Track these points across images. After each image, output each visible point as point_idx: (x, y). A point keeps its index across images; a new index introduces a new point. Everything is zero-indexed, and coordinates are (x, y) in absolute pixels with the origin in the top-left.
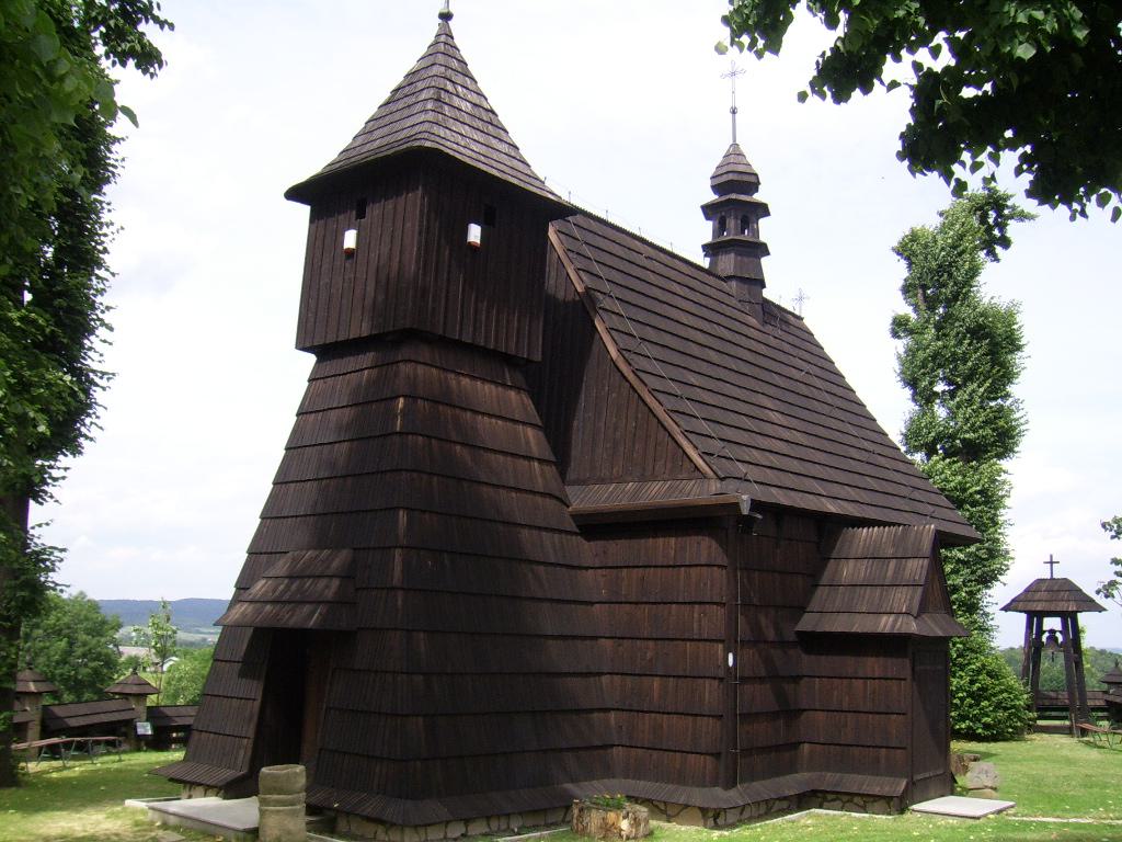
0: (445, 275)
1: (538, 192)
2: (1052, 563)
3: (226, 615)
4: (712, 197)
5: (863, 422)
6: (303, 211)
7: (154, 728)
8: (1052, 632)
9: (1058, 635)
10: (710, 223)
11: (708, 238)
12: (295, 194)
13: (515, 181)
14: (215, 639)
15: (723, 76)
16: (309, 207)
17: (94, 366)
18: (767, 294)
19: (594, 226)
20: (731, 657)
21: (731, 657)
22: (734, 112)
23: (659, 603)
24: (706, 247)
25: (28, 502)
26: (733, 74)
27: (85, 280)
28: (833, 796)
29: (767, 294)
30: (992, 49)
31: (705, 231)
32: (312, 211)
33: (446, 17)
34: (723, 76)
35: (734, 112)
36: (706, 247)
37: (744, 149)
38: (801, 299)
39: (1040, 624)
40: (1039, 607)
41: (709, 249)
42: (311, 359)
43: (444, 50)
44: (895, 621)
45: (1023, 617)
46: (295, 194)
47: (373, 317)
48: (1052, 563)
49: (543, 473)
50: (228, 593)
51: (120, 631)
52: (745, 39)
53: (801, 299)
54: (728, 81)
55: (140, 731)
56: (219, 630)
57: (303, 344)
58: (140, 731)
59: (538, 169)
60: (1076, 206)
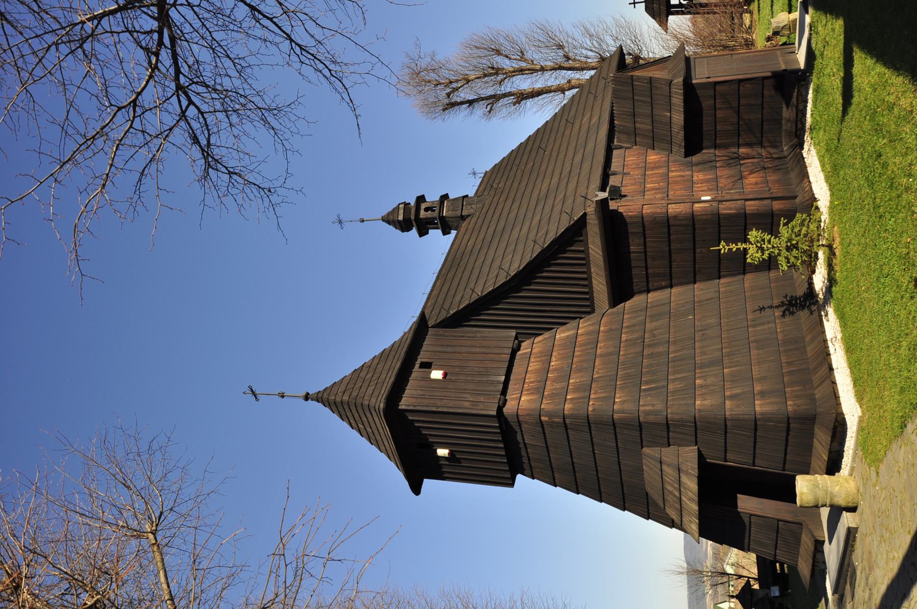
1: (411, 335)
2: (634, 3)
3: (693, 536)
4: (414, 232)
5: (549, 126)
6: (428, 484)
7: (774, 584)
10: (430, 231)
11: (439, 232)
12: (416, 489)
13: (393, 379)
14: (710, 542)
15: (342, 228)
18: (471, 194)
21: (703, 198)
24: (445, 233)
27: (798, 402)
28: (799, 123)
29: (471, 194)
30: (727, 209)
31: (435, 234)
33: (307, 397)
36: (445, 233)
37: (384, 213)
38: (474, 174)
39: (675, 6)
40: (664, 8)
41: (446, 232)
42: (519, 477)
43: (320, 398)
44: (687, 473)
45: (671, 18)
46: (416, 489)
47: (709, 422)
48: (634, 3)
50: (677, 535)
51: (820, 204)
54: (345, 225)
55: (777, 594)
56: (703, 540)
58: (777, 594)
59: (397, 337)
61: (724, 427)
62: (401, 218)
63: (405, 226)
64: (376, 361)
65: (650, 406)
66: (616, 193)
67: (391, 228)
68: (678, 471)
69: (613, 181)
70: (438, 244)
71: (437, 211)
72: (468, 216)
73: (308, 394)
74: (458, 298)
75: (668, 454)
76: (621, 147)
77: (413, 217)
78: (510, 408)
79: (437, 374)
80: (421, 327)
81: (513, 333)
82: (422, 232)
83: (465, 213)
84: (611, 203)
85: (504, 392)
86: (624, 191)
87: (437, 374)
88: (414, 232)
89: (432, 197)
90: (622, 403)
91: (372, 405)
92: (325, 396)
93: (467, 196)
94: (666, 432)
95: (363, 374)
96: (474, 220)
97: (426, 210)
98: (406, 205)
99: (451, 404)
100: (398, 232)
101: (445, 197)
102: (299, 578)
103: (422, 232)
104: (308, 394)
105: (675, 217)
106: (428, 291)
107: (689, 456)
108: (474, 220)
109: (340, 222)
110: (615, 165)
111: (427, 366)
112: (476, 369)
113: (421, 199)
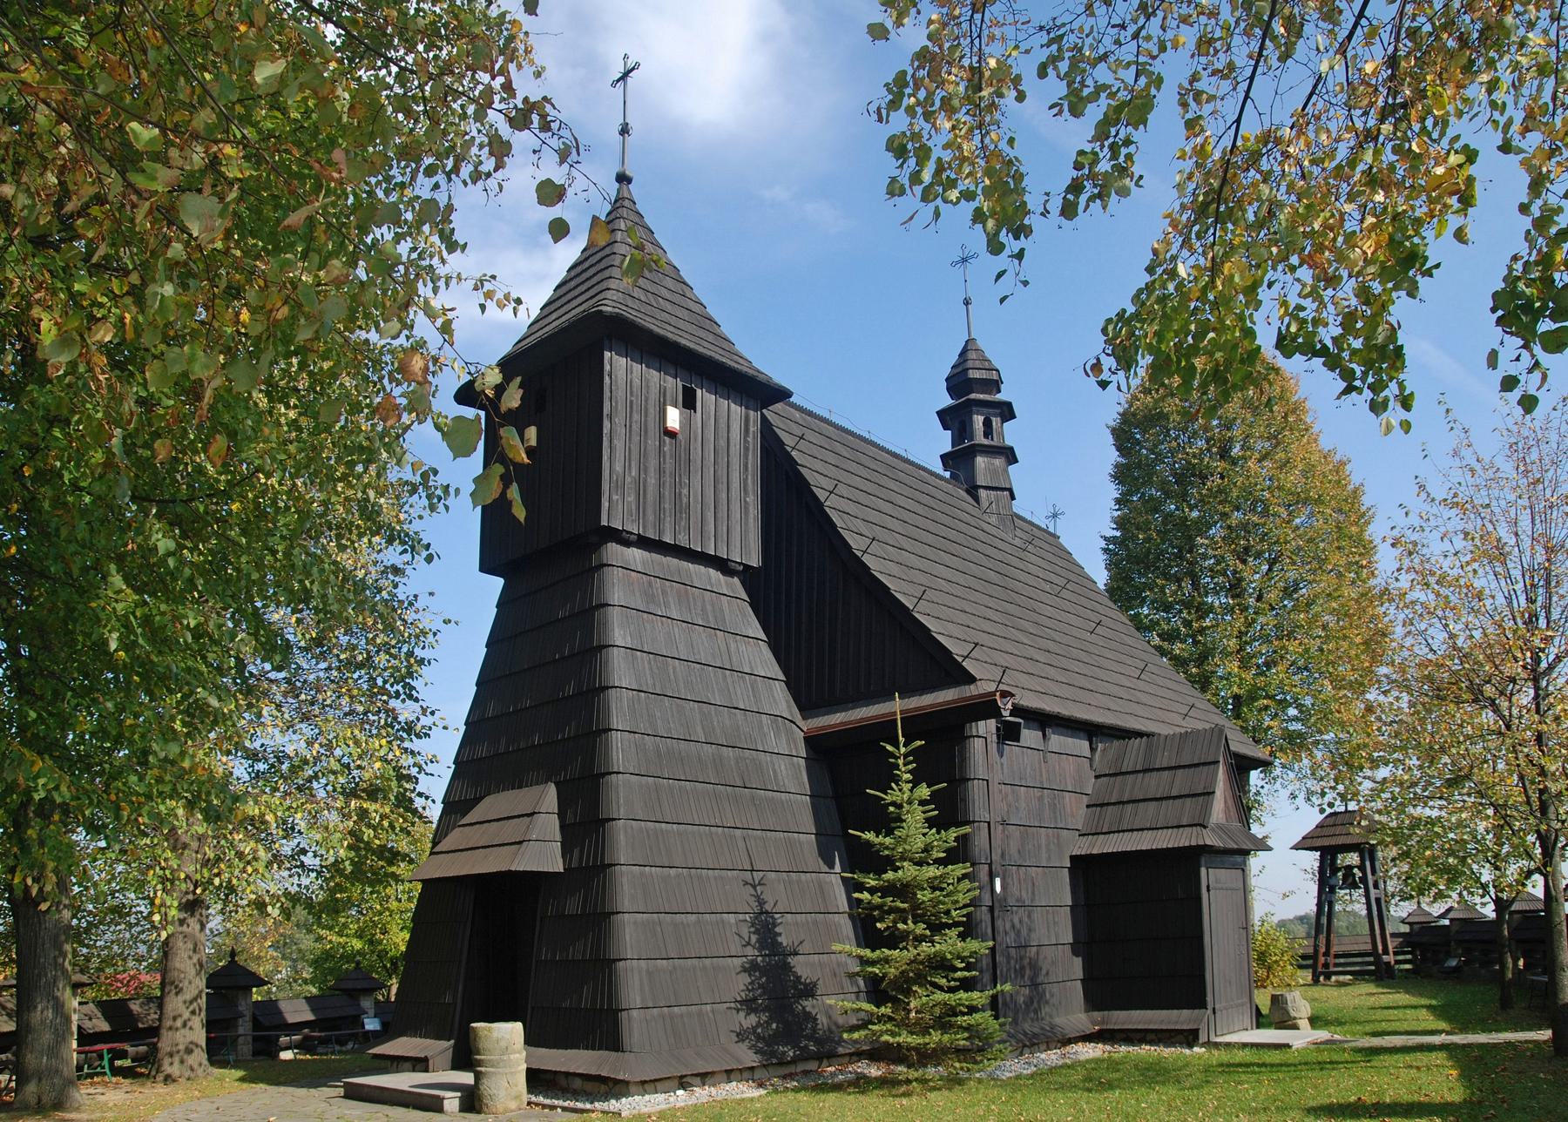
0: (455, 607)
4: (947, 401)
8: (1349, 868)
9: (1356, 870)
11: (948, 448)
12: (1270, 849)
15: (954, 264)
16: (519, 1026)
17: (178, 965)
18: (1018, 507)
19: (873, 451)
20: (998, 888)
21: (998, 882)
22: (967, 302)
23: (1128, 802)
25: (1547, 1028)
26: (964, 260)
29: (1018, 507)
32: (505, 603)
33: (623, 179)
34: (954, 264)
35: (967, 302)
36: (945, 458)
37: (981, 344)
38: (1055, 516)
39: (1334, 859)
42: (498, 583)
46: (1270, 849)
49: (628, 371)
52: (186, 764)
53: (1055, 516)
54: (959, 270)
57: (488, 565)
60: (513, 399)
61: (599, 920)
62: (973, 374)
63: (959, 382)
64: (696, 308)
65: (626, 795)
66: (1009, 733)
67: (954, 359)
68: (528, 836)
69: (1030, 736)
70: (929, 445)
71: (986, 442)
72: (977, 499)
73: (629, 180)
74: (818, 466)
75: (549, 825)
76: (1093, 750)
77: (973, 396)
78: (613, 551)
79: (674, 418)
80: (759, 392)
81: (755, 561)
82: (944, 416)
83: (983, 493)
84: (992, 724)
85: (644, 543)
86: (1011, 749)
87: (674, 418)
88: (947, 401)
89: (1011, 434)
90: (621, 751)
91: (609, 294)
92: (624, 212)
93: (1013, 498)
94: (585, 823)
95: (669, 283)
96: (969, 508)
97: (987, 424)
98: (995, 385)
99: (619, 444)
100: (947, 371)
101: (1010, 456)
102: (635, 427)
103: (944, 416)
104: (629, 180)
105: (966, 789)
106: (834, 419)
107: (544, 855)
108: (969, 508)
109: (964, 260)
110: (1057, 741)
111: (689, 402)
112: (685, 491)
113: (1007, 412)
